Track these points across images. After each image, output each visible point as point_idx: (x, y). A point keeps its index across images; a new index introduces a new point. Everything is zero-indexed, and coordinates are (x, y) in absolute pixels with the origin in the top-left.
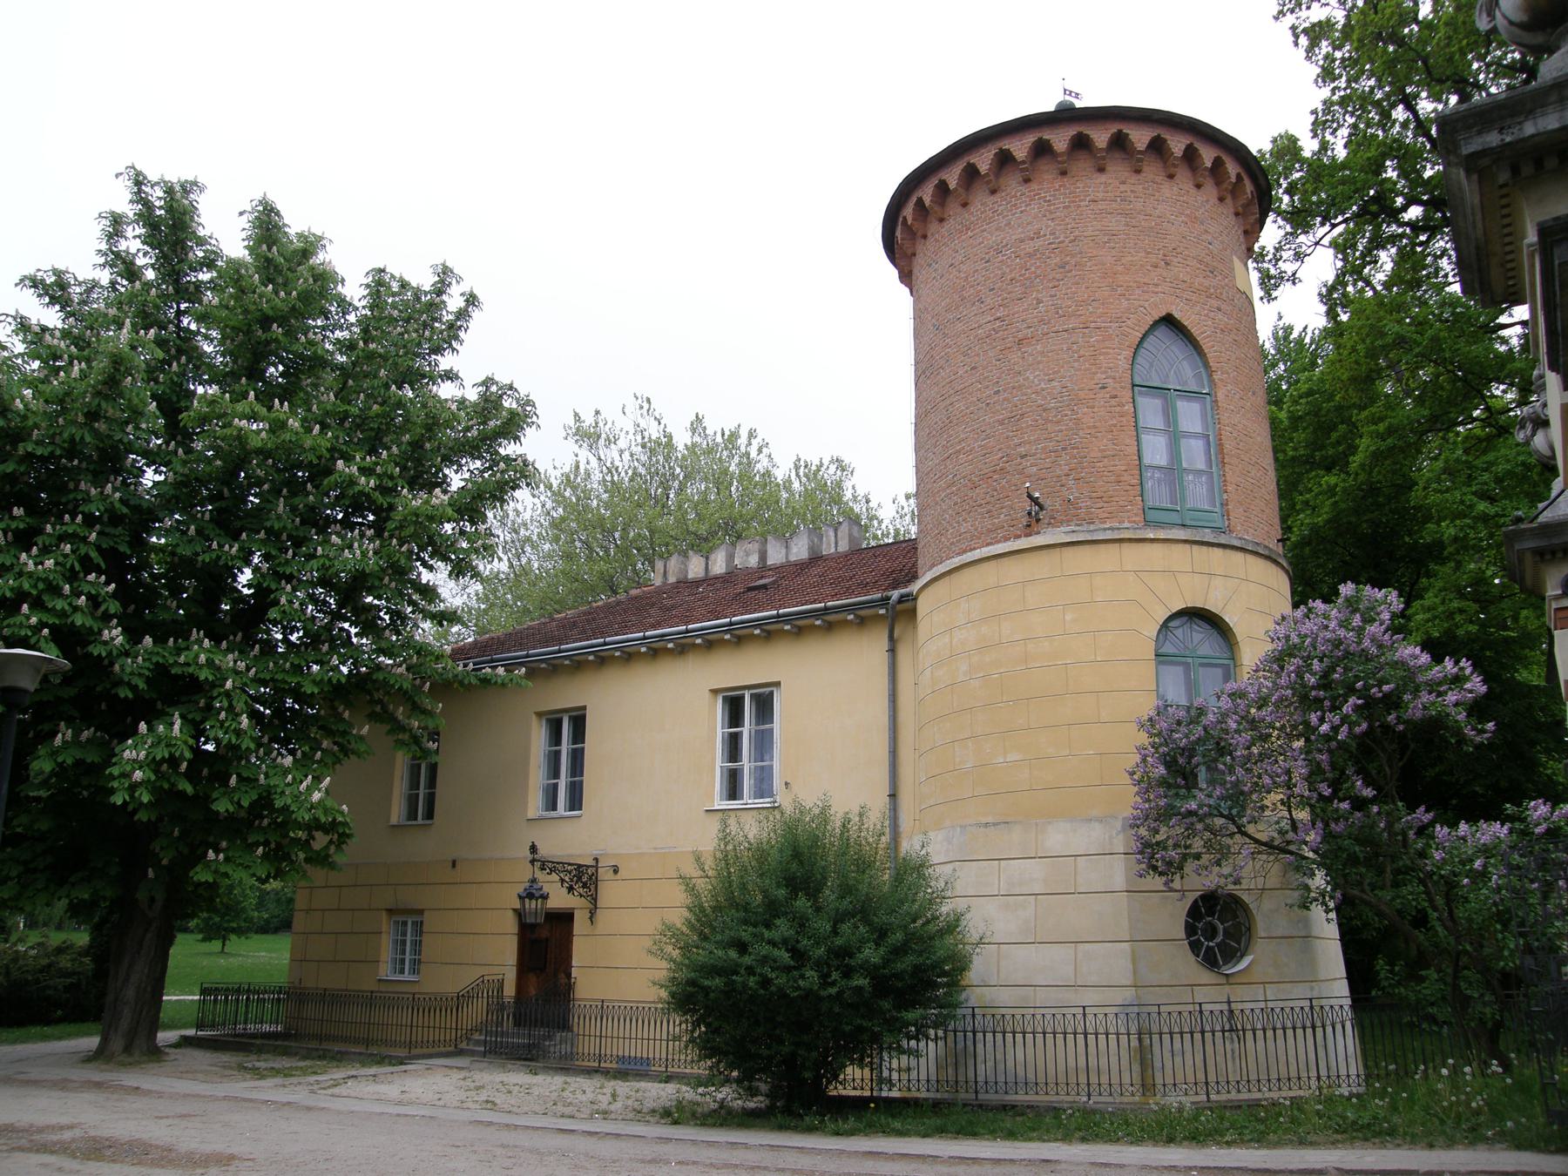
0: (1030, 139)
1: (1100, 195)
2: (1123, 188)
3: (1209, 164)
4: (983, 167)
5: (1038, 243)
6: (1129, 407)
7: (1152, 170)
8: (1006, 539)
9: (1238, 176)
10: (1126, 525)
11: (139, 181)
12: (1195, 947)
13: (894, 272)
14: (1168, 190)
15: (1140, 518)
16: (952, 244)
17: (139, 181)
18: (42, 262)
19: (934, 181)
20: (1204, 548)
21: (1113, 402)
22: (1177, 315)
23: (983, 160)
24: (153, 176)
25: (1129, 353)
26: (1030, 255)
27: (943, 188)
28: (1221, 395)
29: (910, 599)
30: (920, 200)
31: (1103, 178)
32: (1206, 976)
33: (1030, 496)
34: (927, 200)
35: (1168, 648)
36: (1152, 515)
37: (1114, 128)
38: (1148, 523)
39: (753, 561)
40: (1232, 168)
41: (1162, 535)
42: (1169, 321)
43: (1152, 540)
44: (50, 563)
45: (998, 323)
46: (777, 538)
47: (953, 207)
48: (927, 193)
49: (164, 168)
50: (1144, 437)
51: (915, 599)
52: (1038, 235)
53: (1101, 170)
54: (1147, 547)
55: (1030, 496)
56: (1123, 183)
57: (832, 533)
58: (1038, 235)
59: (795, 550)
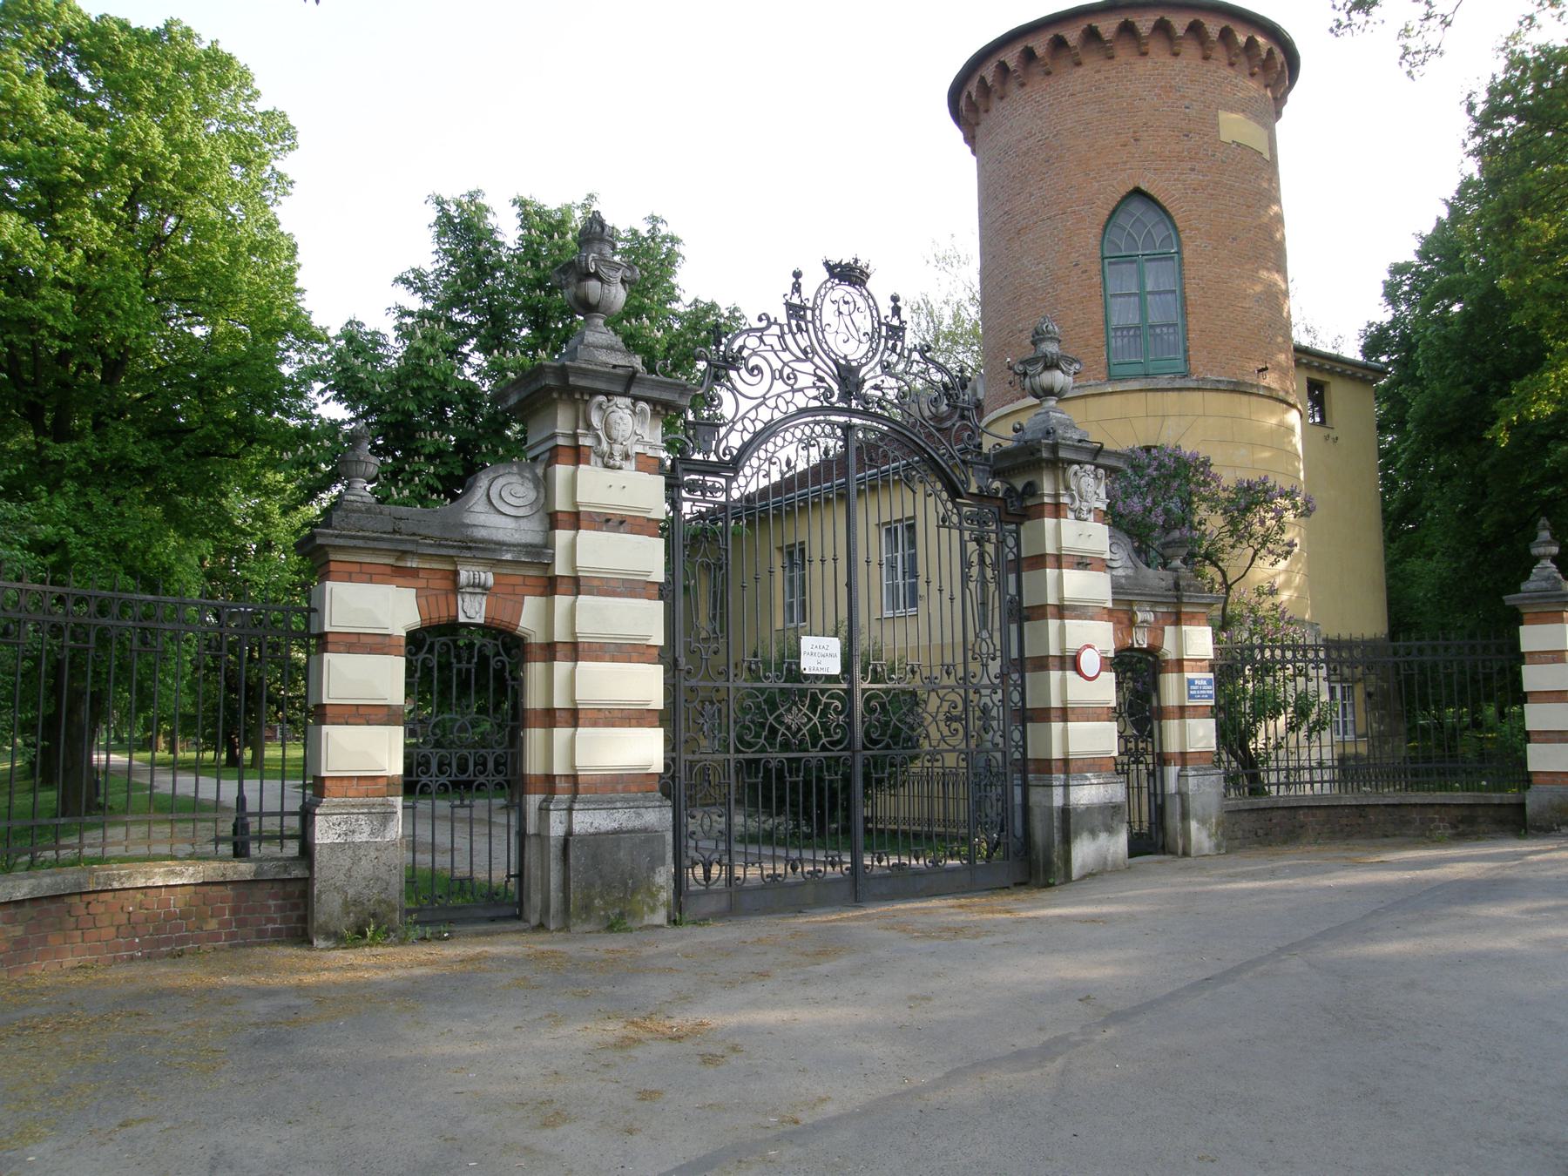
0: (1018, 48)
1: (1078, 88)
2: (1097, 77)
5: (1031, 141)
6: (1097, 279)
7: (1124, 53)
8: (1012, 401)
11: (440, 202)
14: (1142, 67)
16: (1019, 113)
17: (440, 202)
18: (403, 267)
20: (1159, 394)
22: (1143, 187)
23: (1011, 57)
24: (446, 198)
25: (1098, 230)
26: (1025, 154)
27: (1003, 67)
28: (1187, 253)
30: (983, 79)
31: (1081, 71)
34: (989, 80)
36: (1117, 371)
37: (1083, 24)
38: (1111, 379)
41: (1119, 387)
42: (1137, 192)
44: (406, 492)
47: (1012, 86)
48: (989, 71)
49: (454, 191)
50: (1111, 301)
52: (1031, 134)
53: (1078, 64)
54: (1107, 399)
58: (1031, 134)
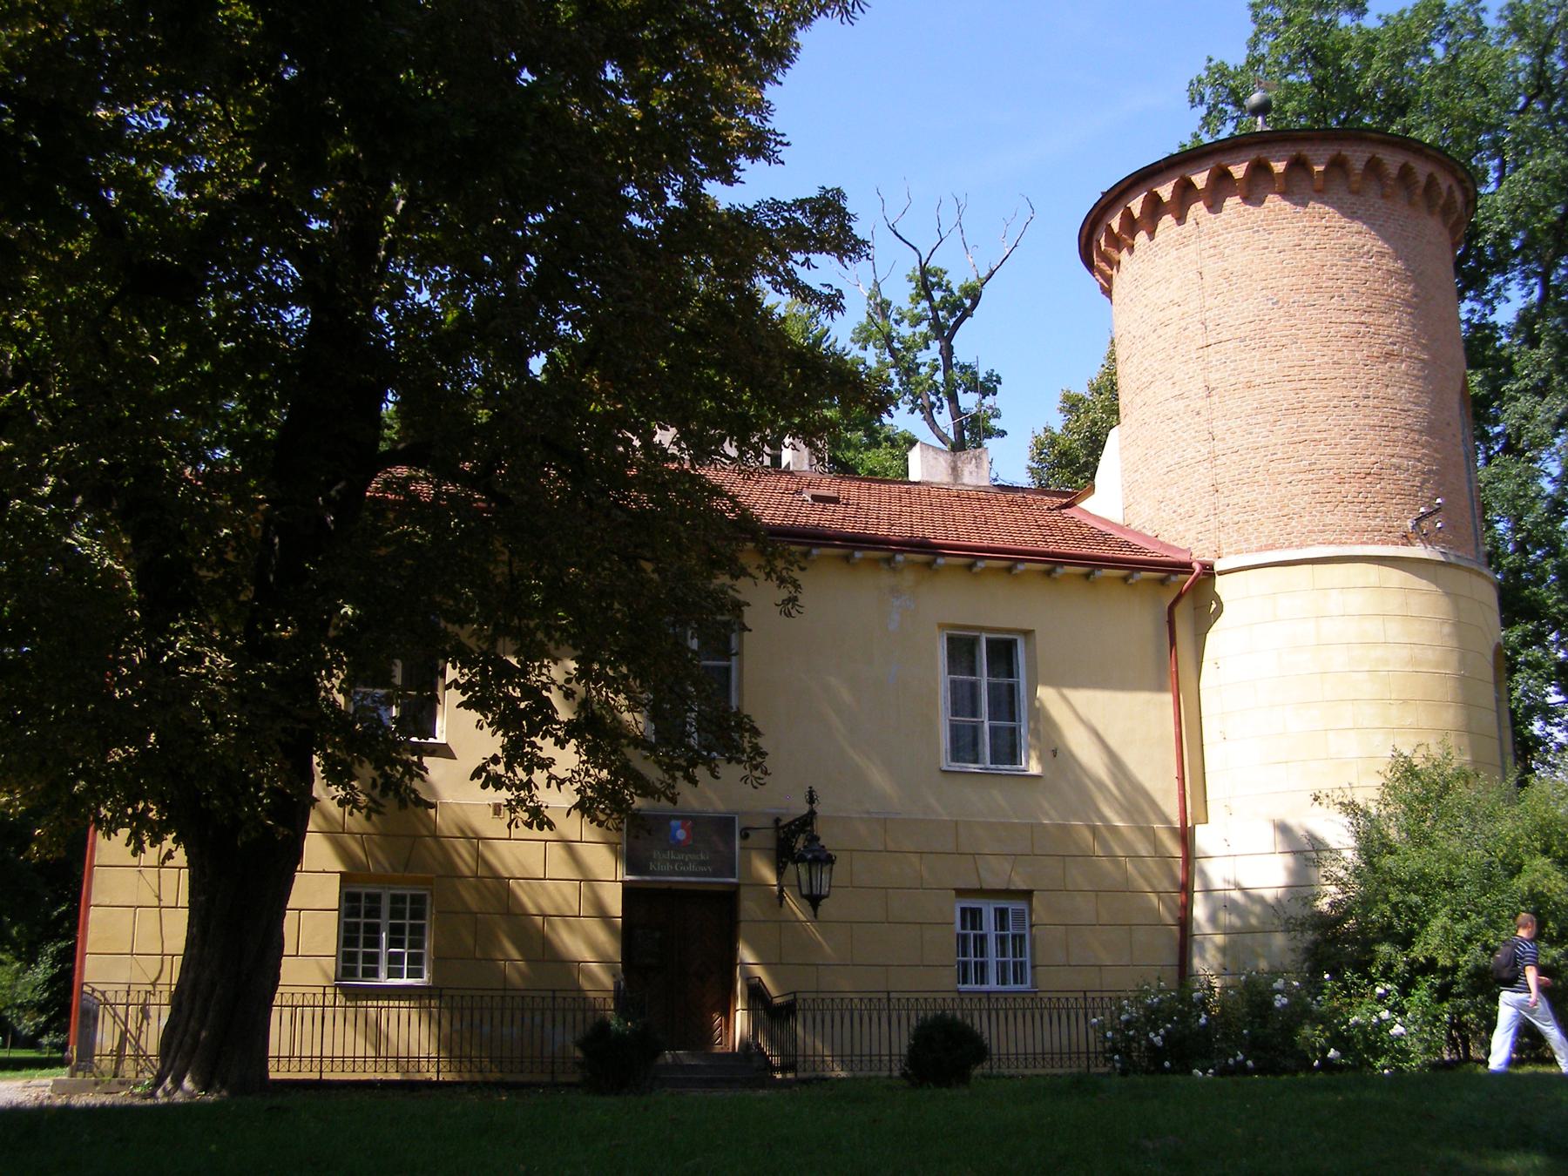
45: (1363, 329)
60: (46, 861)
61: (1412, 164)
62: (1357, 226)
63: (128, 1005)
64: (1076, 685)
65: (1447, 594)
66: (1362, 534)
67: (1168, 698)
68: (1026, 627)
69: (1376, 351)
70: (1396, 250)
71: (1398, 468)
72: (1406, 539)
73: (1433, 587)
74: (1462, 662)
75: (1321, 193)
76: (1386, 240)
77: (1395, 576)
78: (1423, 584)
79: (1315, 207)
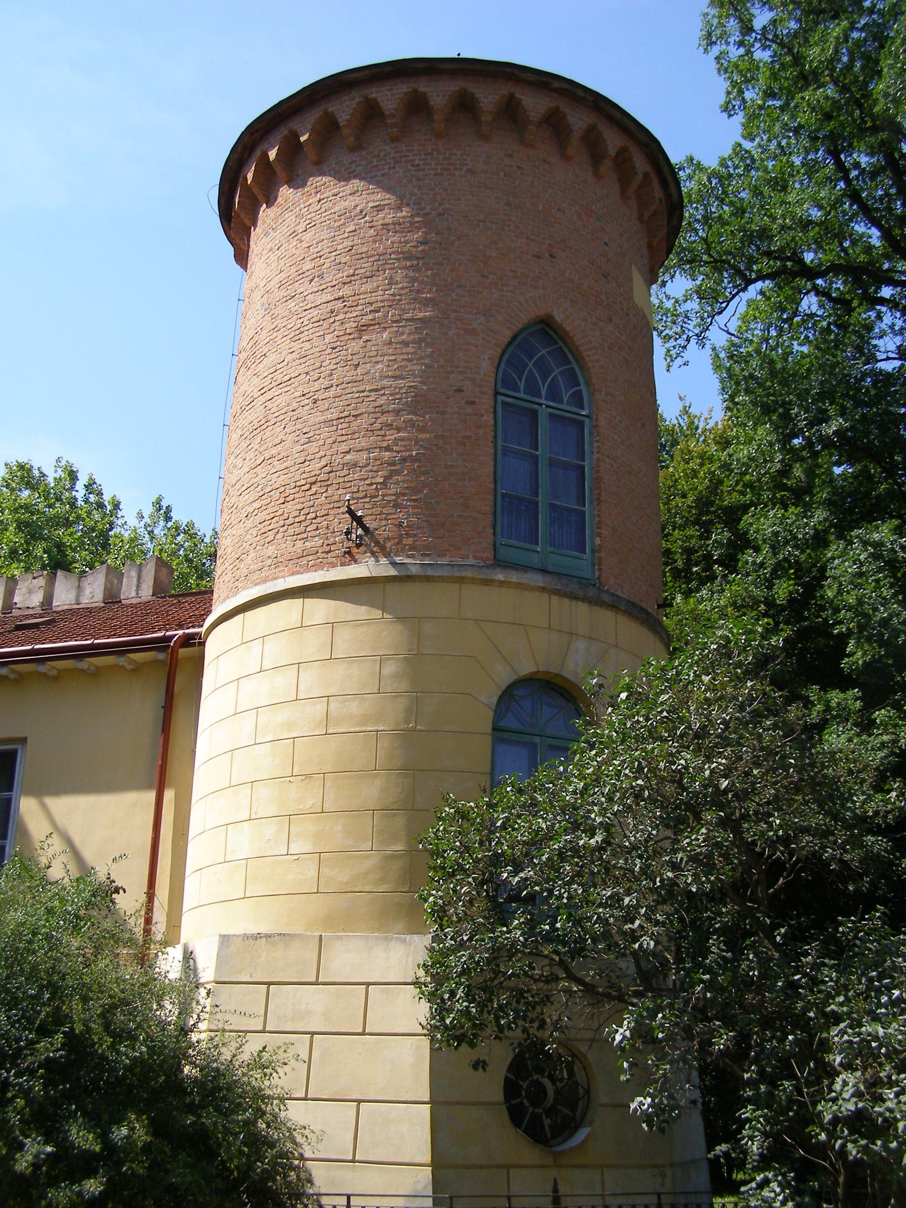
3: (612, 152)
4: (343, 118)
9: (646, 176)
10: (471, 561)
12: (516, 1116)
13: (231, 250)
15: (490, 554)
19: (283, 131)
21: (469, 409)
29: (195, 643)
32: (529, 1153)
33: (351, 512)
35: (510, 722)
37: (505, 89)
39: (37, 599)
40: (641, 164)
43: (502, 584)
45: (339, 304)
46: (901, 1162)
51: (203, 644)
55: (351, 512)
56: (510, 156)
57: (134, 574)
59: (87, 591)
60: (634, 1028)
61: (422, 89)
62: (356, 184)
63: (603, 1195)
64: (58, 791)
65: (400, 619)
66: (298, 562)
67: (152, 795)
68: (20, 734)
69: (350, 326)
70: (401, 198)
71: (355, 465)
72: (349, 557)
73: (377, 613)
74: (414, 710)
75: (320, 166)
76: (389, 189)
77: (320, 609)
78: (361, 612)
79: (315, 181)
